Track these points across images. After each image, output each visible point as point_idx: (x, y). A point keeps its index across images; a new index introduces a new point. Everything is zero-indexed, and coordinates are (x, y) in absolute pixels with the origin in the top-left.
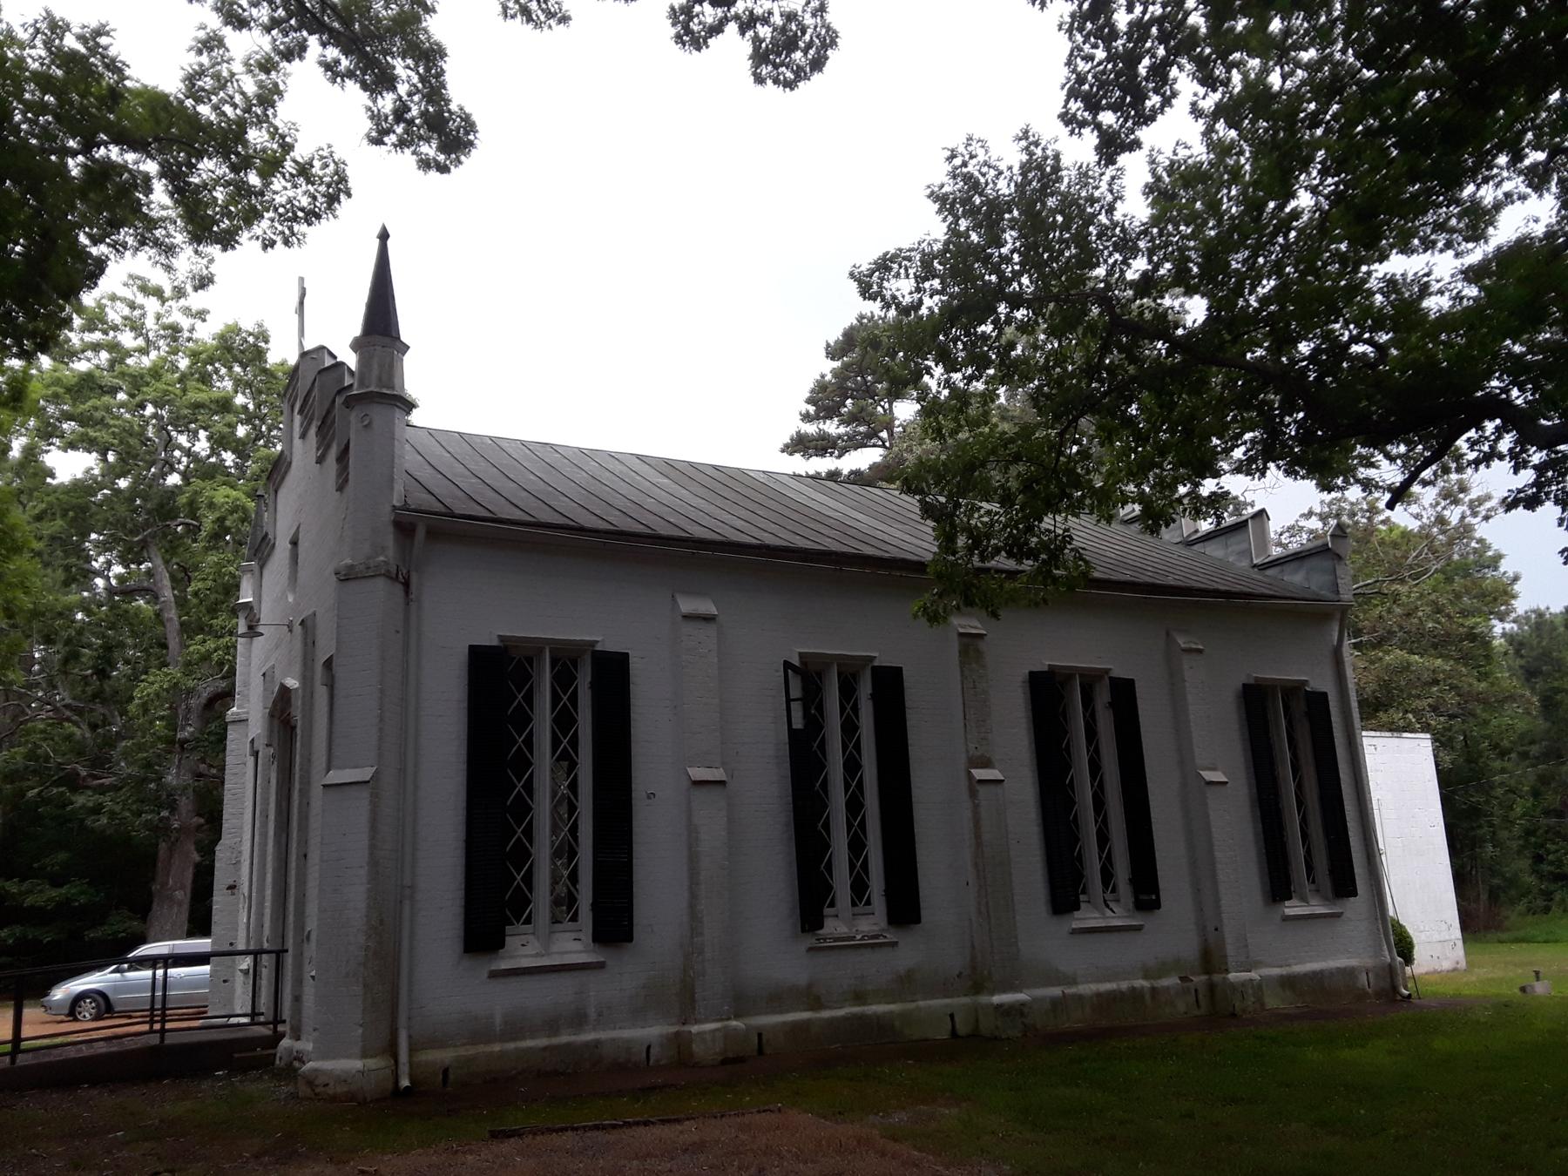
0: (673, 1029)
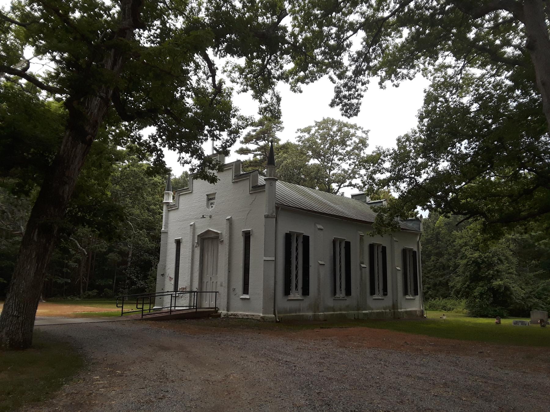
0: (314, 314)
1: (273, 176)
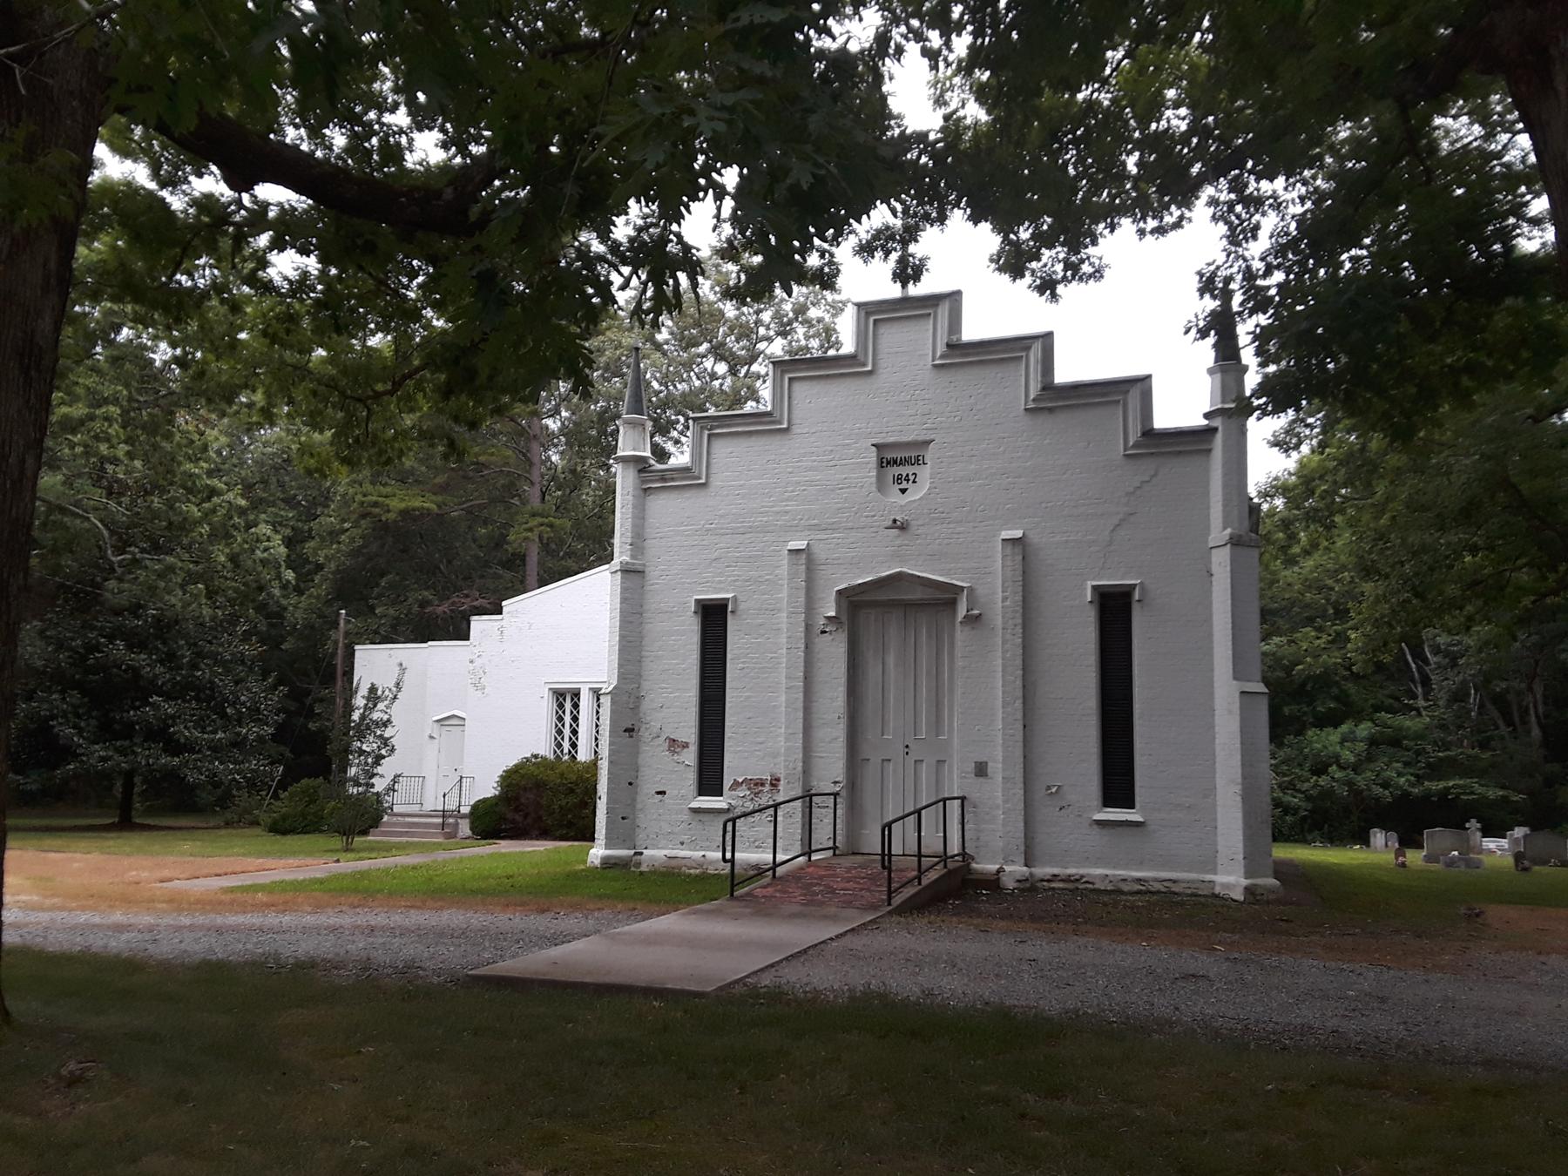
1: (646, 414)
